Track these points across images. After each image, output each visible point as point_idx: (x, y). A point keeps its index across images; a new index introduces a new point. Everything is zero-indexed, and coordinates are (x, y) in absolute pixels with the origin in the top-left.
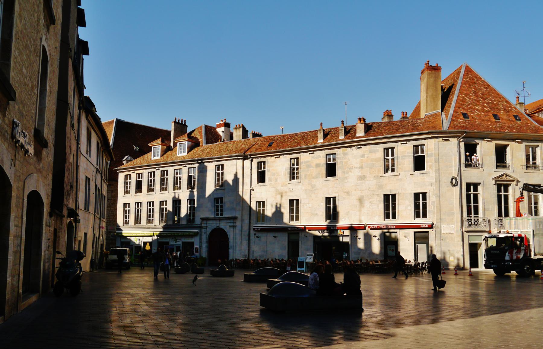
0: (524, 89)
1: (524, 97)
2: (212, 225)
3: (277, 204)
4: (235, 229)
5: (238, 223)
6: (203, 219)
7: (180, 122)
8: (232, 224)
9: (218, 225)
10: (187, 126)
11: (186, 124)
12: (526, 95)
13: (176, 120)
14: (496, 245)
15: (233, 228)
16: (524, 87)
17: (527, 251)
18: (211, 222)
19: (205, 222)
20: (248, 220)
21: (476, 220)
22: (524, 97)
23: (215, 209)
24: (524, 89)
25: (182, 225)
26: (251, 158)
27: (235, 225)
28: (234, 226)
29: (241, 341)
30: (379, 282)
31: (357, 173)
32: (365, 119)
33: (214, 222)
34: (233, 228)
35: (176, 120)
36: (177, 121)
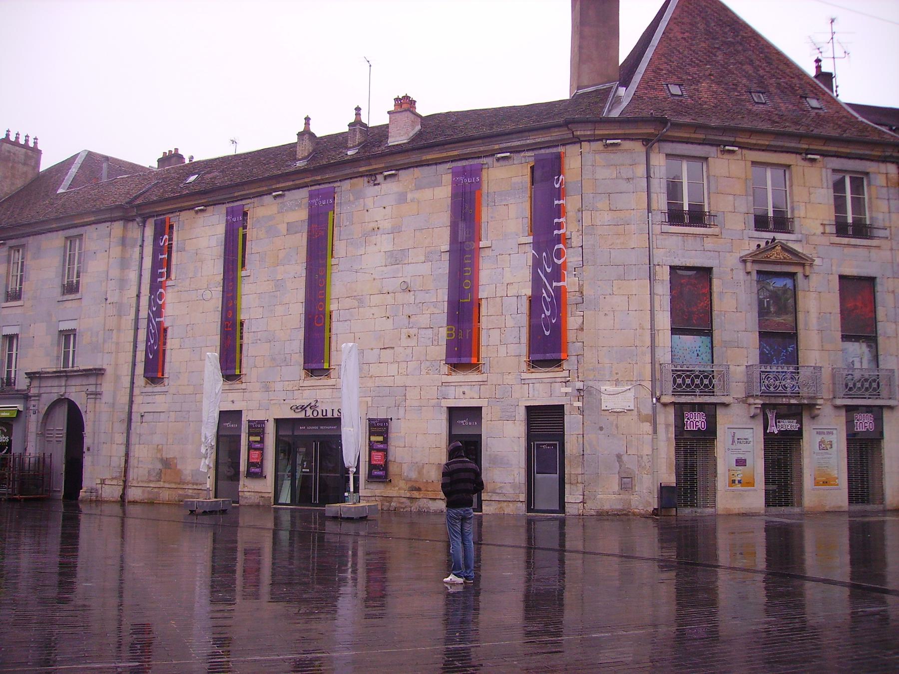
0: (832, 38)
1: (834, 58)
2: (52, 391)
4: (98, 401)
5: (107, 386)
6: (31, 376)
10: (39, 152)
11: (39, 148)
12: (839, 53)
14: (321, 138)
15: (96, 399)
16: (833, 33)
17: (189, 503)
18: (49, 383)
19: (36, 383)
21: (697, 373)
22: (834, 58)
24: (832, 38)
31: (385, 243)
32: (415, 102)
33: (56, 382)
34: (96, 399)
35: (8, 135)
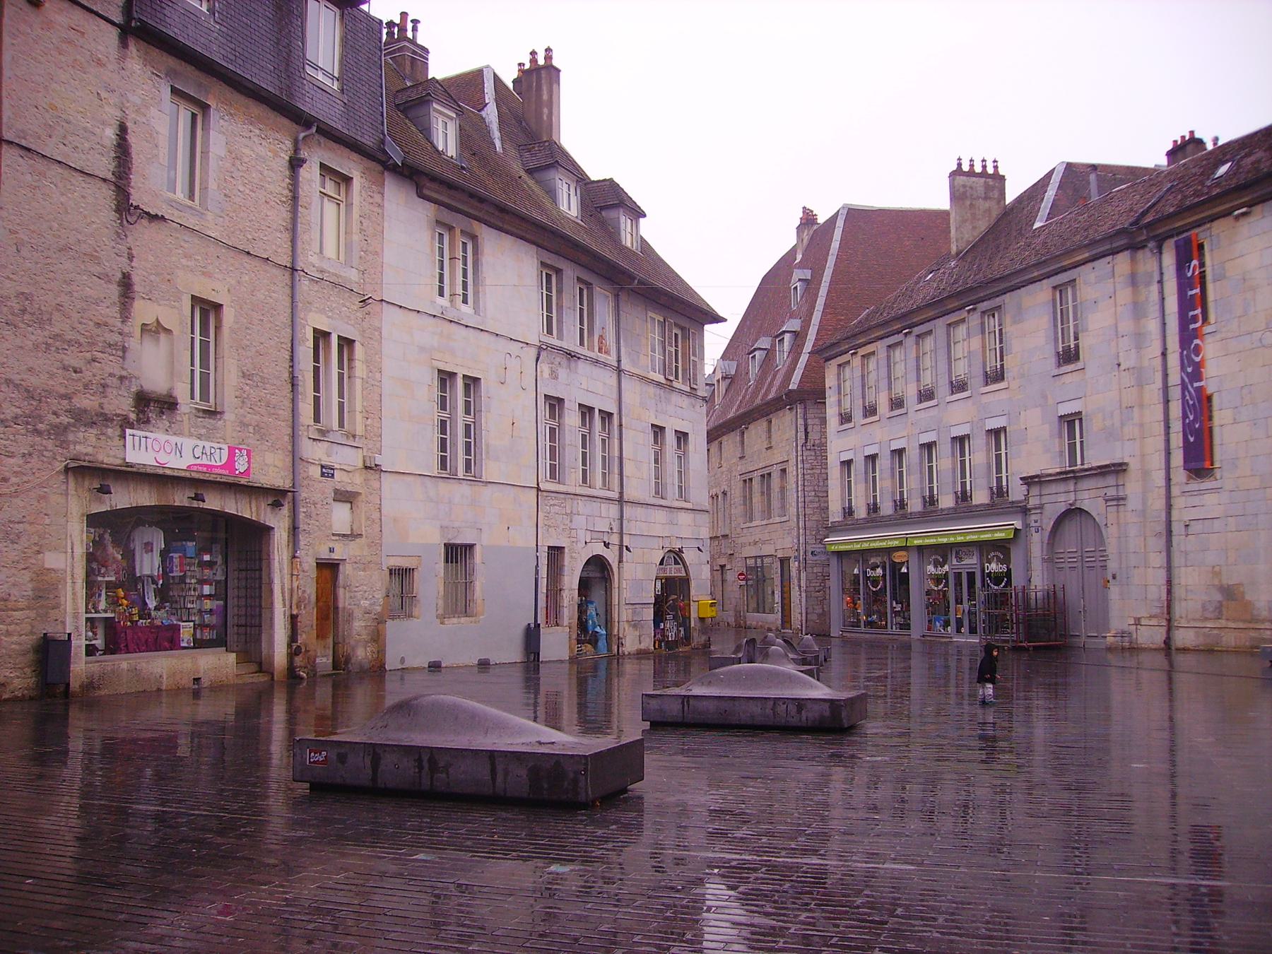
3: (533, 53)
5: (1132, 487)
6: (1029, 481)
7: (978, 169)
8: (1112, 492)
9: (1072, 497)
10: (1002, 178)
11: (1001, 172)
13: (960, 165)
18: (1053, 488)
19: (1035, 490)
20: (1162, 473)
23: (1061, 445)
25: (977, 506)
26: (1154, 237)
27: (1121, 494)
28: (1118, 499)
29: (45, 836)
30: (1078, 518)
33: (1061, 487)
35: (960, 165)
36: (966, 168)
